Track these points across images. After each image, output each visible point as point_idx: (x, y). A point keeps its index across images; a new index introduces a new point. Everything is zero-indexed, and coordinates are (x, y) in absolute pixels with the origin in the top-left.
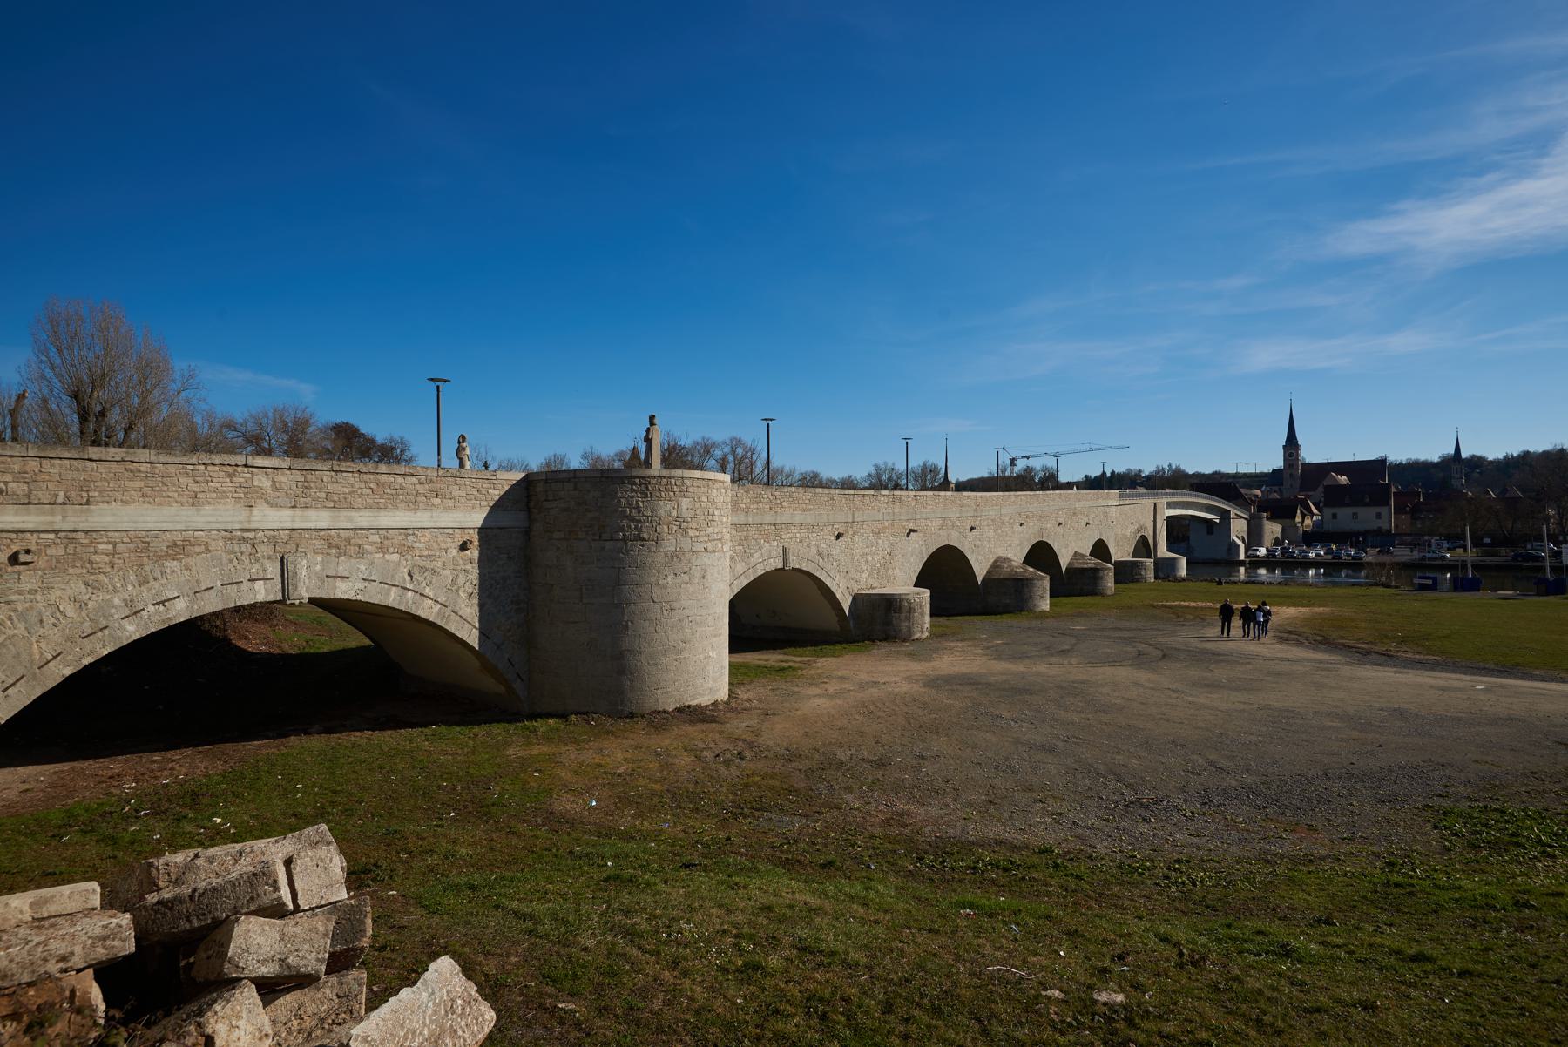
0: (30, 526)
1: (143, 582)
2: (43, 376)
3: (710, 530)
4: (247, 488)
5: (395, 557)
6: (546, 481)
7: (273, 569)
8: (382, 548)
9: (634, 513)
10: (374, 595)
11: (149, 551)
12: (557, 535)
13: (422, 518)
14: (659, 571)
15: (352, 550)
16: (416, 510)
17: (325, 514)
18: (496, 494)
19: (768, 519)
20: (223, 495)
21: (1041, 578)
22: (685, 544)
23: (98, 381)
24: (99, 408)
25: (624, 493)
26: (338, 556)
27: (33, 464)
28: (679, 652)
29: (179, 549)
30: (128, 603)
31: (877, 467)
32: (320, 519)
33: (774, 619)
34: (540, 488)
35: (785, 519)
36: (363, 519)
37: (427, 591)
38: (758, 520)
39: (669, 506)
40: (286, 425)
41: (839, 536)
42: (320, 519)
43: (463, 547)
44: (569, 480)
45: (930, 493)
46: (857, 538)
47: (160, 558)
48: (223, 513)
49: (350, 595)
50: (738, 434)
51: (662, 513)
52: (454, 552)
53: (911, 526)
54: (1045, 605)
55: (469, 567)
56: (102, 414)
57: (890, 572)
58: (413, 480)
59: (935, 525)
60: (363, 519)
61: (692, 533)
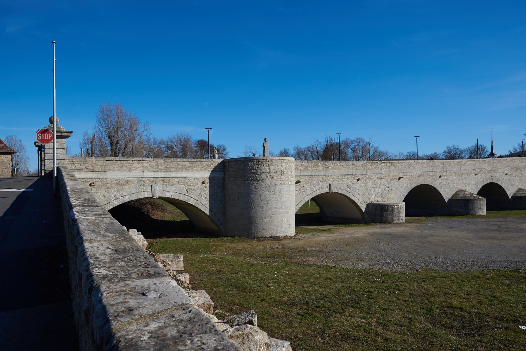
0: (94, 177)
1: (118, 191)
2: (100, 130)
3: (283, 177)
4: (143, 166)
5: (182, 186)
6: (229, 162)
7: (149, 189)
8: (179, 183)
9: (254, 171)
10: (176, 197)
11: (121, 183)
12: (232, 179)
13: (190, 174)
14: (263, 191)
15: (170, 183)
16: (188, 172)
17: (163, 173)
18: (213, 167)
19: (322, 173)
20: (137, 168)
21: (479, 199)
22: (273, 182)
23: (116, 132)
24: (116, 140)
25: (251, 165)
26: (166, 185)
27: (94, 162)
28: (271, 218)
29: (126, 183)
30: (115, 196)
31: (449, 148)
32: (161, 174)
33: (325, 212)
34: (227, 164)
35: (330, 173)
36: (173, 174)
37: (192, 196)
38: (317, 174)
39: (266, 169)
40: (181, 142)
41: (358, 180)
42: (161, 174)
43: (203, 183)
44: (235, 161)
45: (413, 161)
46: (368, 181)
47: (122, 185)
48: (137, 173)
49: (170, 196)
50: (360, 136)
51: (264, 171)
52: (200, 184)
53: (401, 175)
54: (483, 212)
55: (205, 189)
56: (117, 142)
57: (389, 195)
58: (188, 163)
59: (416, 175)
60: (173, 174)
61: (275, 178)
